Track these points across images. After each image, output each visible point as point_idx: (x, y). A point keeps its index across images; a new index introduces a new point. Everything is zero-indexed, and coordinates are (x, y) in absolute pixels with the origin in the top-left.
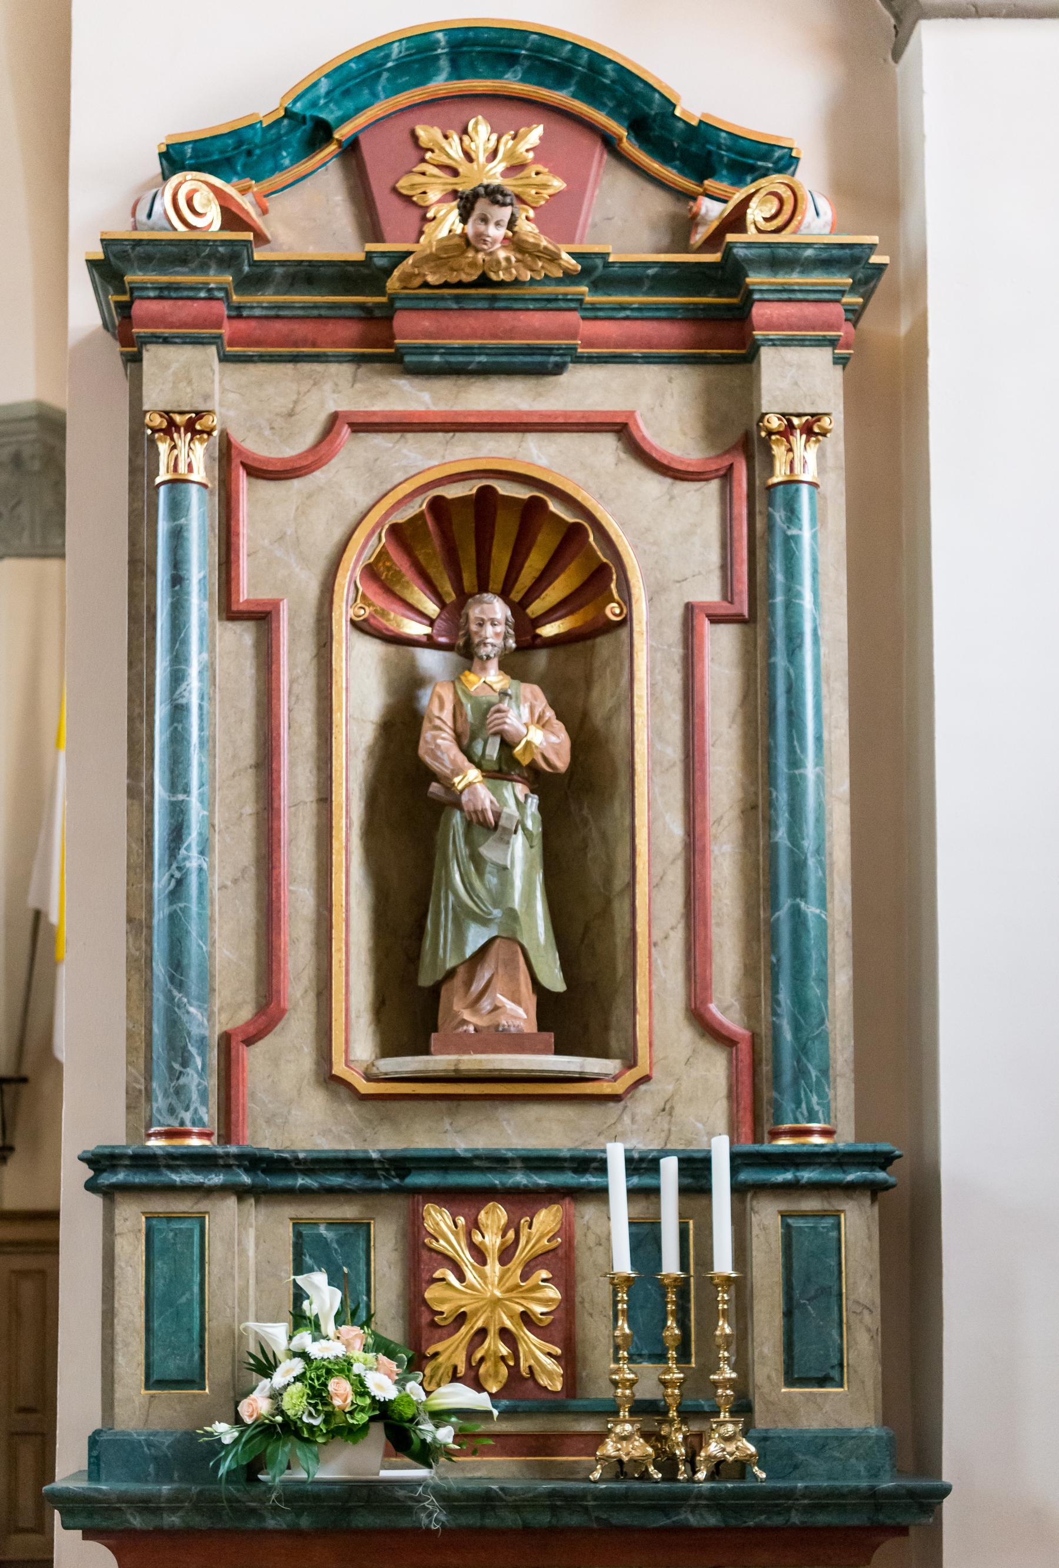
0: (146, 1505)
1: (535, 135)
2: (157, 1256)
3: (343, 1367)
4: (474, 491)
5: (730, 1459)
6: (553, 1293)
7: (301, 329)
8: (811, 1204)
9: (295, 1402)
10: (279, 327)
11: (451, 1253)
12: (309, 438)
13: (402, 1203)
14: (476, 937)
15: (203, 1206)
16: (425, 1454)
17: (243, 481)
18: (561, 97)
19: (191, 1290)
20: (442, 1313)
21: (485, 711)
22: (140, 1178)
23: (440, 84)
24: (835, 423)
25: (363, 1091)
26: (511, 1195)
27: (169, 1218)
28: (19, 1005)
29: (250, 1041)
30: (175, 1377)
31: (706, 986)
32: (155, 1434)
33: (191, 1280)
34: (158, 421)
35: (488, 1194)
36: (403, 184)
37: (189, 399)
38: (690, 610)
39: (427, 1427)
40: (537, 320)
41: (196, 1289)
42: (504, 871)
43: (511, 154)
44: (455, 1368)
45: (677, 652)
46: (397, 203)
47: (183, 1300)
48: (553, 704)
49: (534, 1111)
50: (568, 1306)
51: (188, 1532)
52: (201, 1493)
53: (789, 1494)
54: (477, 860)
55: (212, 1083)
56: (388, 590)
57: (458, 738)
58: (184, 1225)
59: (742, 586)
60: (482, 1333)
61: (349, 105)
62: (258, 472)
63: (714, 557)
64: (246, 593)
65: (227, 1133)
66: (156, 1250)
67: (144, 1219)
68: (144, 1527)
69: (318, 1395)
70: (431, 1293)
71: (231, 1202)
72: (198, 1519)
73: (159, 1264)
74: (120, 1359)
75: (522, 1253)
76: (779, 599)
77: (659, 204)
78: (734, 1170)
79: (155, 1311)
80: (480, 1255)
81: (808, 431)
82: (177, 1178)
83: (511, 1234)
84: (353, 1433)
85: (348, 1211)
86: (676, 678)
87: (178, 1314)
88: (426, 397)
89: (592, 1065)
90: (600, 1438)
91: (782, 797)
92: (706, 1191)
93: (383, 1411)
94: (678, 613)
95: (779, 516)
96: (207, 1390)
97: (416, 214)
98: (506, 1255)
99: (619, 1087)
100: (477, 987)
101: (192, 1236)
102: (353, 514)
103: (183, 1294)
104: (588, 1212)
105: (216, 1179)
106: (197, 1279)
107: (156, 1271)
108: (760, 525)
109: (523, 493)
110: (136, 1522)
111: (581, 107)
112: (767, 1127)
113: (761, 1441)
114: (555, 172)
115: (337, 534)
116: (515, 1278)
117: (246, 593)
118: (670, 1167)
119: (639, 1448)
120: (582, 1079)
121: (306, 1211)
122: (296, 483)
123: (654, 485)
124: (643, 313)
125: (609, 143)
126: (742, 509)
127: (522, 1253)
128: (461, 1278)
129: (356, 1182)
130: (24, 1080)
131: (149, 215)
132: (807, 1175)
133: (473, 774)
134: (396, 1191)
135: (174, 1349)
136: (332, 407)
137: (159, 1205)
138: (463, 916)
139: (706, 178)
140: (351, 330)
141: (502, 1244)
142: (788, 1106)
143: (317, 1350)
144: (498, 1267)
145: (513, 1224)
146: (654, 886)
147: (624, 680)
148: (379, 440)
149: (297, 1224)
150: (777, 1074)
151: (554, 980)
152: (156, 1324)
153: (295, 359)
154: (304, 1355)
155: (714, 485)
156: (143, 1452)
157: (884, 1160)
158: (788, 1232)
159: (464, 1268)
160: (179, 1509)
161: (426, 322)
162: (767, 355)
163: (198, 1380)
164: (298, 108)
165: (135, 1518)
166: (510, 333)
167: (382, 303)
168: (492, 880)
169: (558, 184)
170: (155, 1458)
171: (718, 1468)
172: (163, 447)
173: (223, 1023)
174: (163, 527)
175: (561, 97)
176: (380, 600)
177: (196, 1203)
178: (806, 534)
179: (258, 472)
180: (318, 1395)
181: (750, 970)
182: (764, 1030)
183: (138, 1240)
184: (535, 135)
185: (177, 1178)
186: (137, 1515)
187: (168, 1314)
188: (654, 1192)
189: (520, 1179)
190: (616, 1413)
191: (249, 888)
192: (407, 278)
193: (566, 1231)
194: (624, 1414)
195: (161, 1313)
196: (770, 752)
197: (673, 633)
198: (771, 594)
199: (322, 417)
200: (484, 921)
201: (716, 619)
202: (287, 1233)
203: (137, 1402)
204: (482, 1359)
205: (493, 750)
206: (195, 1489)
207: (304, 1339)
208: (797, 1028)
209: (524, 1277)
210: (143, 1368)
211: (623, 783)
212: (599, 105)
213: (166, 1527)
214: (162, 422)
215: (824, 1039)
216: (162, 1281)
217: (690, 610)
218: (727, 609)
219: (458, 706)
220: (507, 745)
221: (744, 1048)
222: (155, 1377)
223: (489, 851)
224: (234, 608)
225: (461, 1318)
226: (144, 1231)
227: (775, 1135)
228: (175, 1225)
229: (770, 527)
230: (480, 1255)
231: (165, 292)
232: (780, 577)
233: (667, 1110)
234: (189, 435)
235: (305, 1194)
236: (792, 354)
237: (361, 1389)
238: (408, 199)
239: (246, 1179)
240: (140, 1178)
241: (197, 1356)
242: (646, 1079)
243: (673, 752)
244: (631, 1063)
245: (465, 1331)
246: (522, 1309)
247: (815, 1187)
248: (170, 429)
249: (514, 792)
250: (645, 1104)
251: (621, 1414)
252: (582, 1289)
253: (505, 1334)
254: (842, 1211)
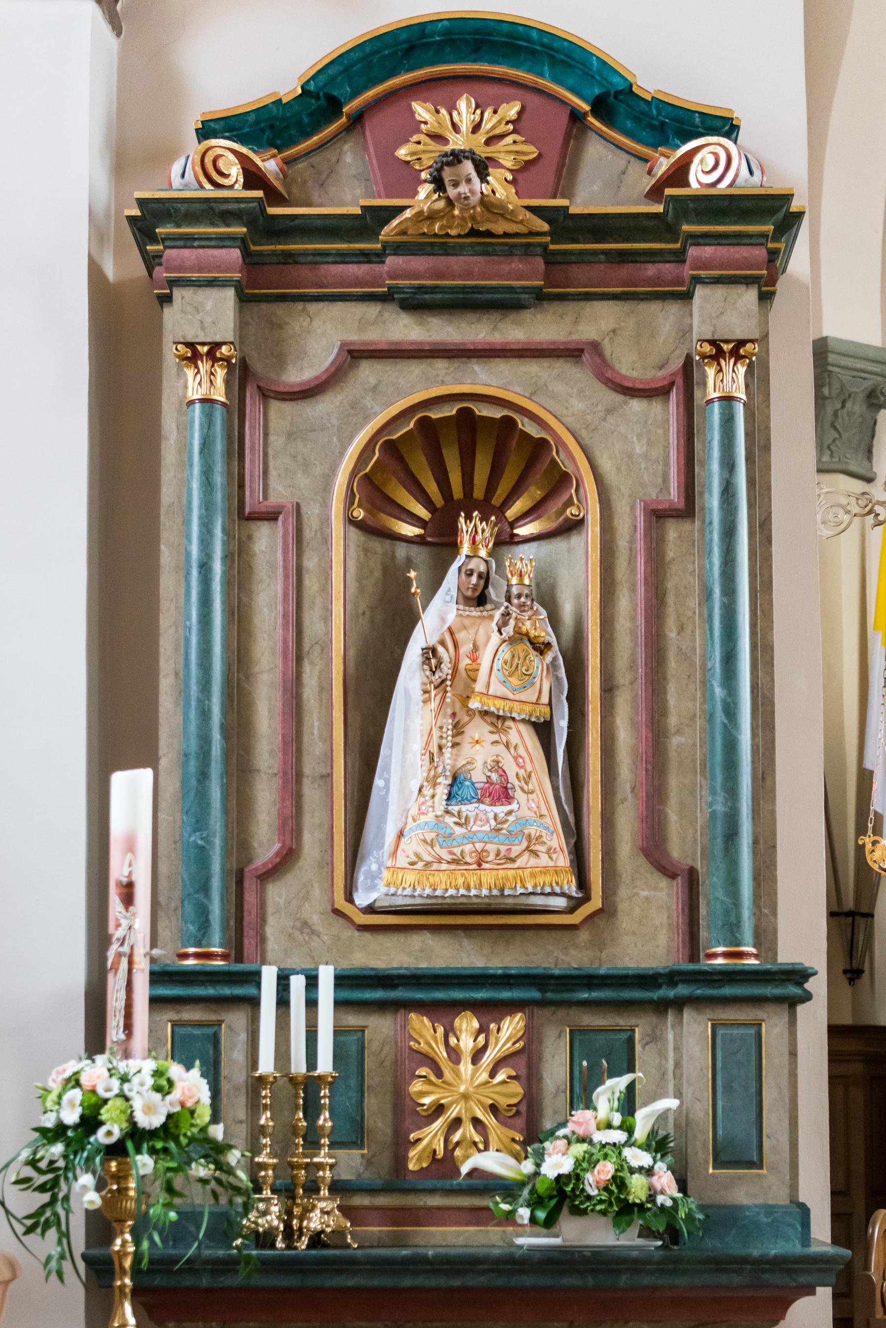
4: (454, 412)
5: (329, 1230)
11: (432, 1054)
20: (423, 1105)
24: (171, 353)
26: (475, 1006)
44: (435, 1151)
60: (457, 1123)
83: (481, 1039)
98: (477, 1056)
116: (484, 1076)
128: (439, 1074)
131: (183, 176)
139: (660, 146)
141: (474, 1046)
144: (470, 1067)
159: (441, 1064)
163: (758, 1163)
164: (312, 87)
167: (677, 249)
171: (317, 1240)
172: (711, 372)
184: (512, 110)
190: (318, 1190)
194: (324, 1192)
204: (458, 1144)
209: (492, 1074)
214: (711, 350)
224: (681, 505)
230: (454, 1055)
234: (732, 361)
246: (491, 1102)
248: (718, 356)
251: (322, 1192)
254: (763, 1020)
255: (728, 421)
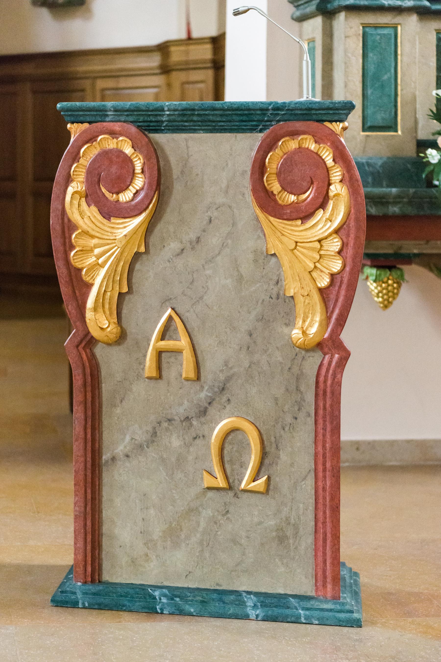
2: (369, 50)
15: (398, 19)
19: (390, 71)
27: (376, 27)
30: (381, 124)
32: (371, 158)
33: (390, 66)
41: (393, 71)
47: (386, 77)
51: (404, 217)
52: (415, 193)
58: (385, 31)
66: (369, 47)
67: (361, 28)
68: (377, 214)
72: (410, 209)
73: (371, 55)
79: (369, 84)
87: (382, 87)
96: (400, 132)
101: (390, 39)
103: (386, 73)
106: (393, 65)
107: (370, 59)
135: (380, 107)
152: (369, 92)
156: (365, 170)
160: (399, 202)
163: (394, 126)
165: (372, 209)
170: (372, 174)
177: (393, 18)
183: (359, 40)
186: (373, 206)
187: (376, 85)
195: (372, 86)
203: (358, 140)
206: (412, 191)
210: (361, 119)
213: (390, 214)
216: (373, 66)
222: (369, 124)
226: (361, 35)
228: (380, 31)
241: (393, 111)
255: (159, 126)
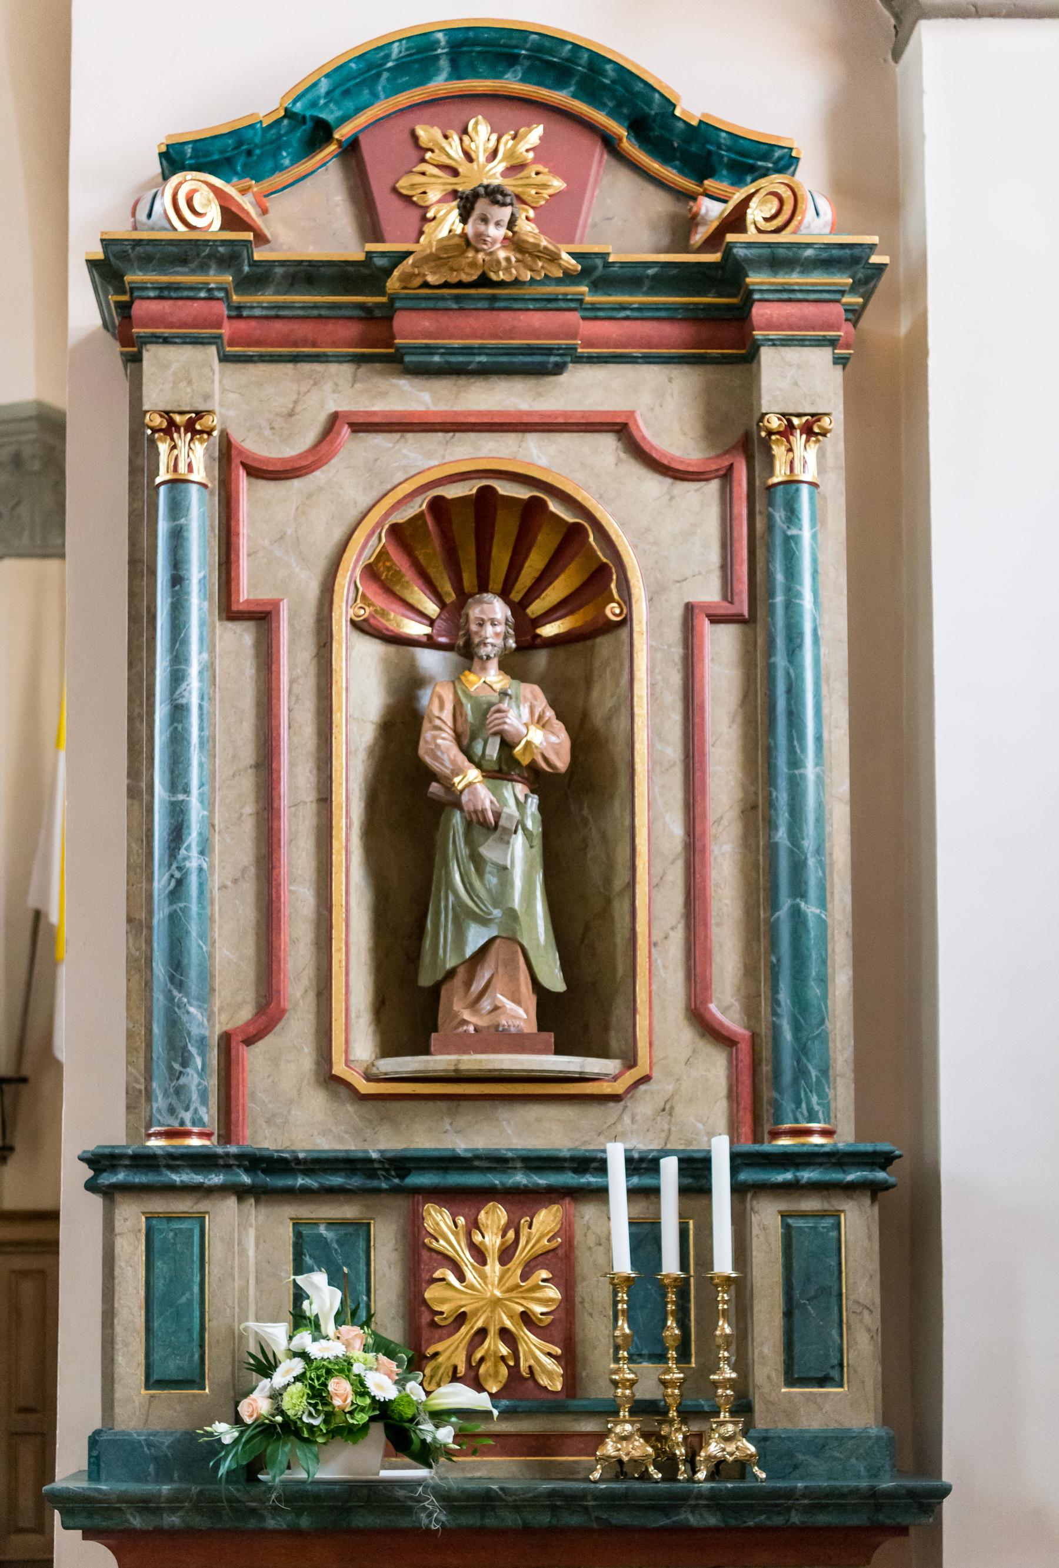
0: (146, 1505)
1: (535, 135)
2: (157, 1256)
3: (343, 1367)
4: (474, 491)
5: (730, 1459)
6: (553, 1293)
7: (301, 329)
8: (811, 1204)
9: (295, 1402)
10: (279, 327)
11: (451, 1253)
12: (309, 438)
13: (402, 1203)
14: (476, 937)
15: (203, 1206)
16: (425, 1454)
17: (243, 481)
18: (561, 97)
19: (191, 1290)
20: (442, 1313)
21: (485, 711)
22: (140, 1178)
23: (440, 84)
24: (835, 423)
25: (363, 1091)
26: (511, 1195)
27: (169, 1218)
28: (19, 1005)
29: (250, 1041)
30: (175, 1377)
31: (706, 986)
32: (155, 1434)
33: (191, 1280)
34: (158, 421)
35: (488, 1194)
36: (403, 184)
37: (189, 399)
38: (690, 610)
39: (427, 1427)
40: (537, 320)
41: (196, 1289)
42: (504, 871)
43: (511, 154)
44: (455, 1368)
45: (677, 652)
46: (397, 203)
47: (183, 1300)
48: (553, 704)
49: (534, 1111)
50: (568, 1306)
51: (188, 1532)
52: (201, 1493)
53: (789, 1494)
54: (477, 860)
55: (212, 1083)
56: (388, 590)
57: (458, 738)
58: (184, 1225)
59: (742, 586)
60: (482, 1333)
61: (349, 105)
62: (258, 472)
63: (714, 557)
64: (246, 593)
65: (227, 1133)
66: (156, 1250)
67: (144, 1219)
68: (144, 1527)
69: (318, 1395)
70: (431, 1293)
71: (231, 1202)
72: (198, 1519)
73: (159, 1264)
74: (120, 1359)
75: (522, 1253)
76: (779, 599)
77: (659, 204)
78: (734, 1170)
79: (155, 1311)
80: (480, 1255)
81: (808, 431)
82: (177, 1178)
83: (511, 1234)
84: (353, 1433)
85: (348, 1211)
86: (676, 678)
87: (178, 1314)
88: (426, 397)
89: (592, 1065)
90: (600, 1438)
91: (782, 797)
92: (706, 1191)
93: (383, 1411)
94: (678, 613)
95: (779, 516)
96: (207, 1390)
97: (416, 214)
98: (506, 1255)
99: (619, 1087)
100: (477, 987)
101: (192, 1236)
102: (353, 514)
103: (183, 1294)
104: (588, 1212)
105: (216, 1179)
106: (197, 1279)
107: (156, 1271)
108: (760, 525)
109: (523, 493)
110: (136, 1522)
111: (581, 107)
112: (767, 1127)
113: (761, 1441)
114: (555, 172)
115: (337, 534)
116: (515, 1278)
117: (246, 593)
118: (670, 1167)
119: (639, 1448)
120: (582, 1079)
121: (306, 1211)
122: (296, 483)
123: (654, 485)
124: (643, 313)
125: (609, 143)
126: (742, 509)
127: (522, 1253)
128: (461, 1278)
129: (356, 1182)
130: (24, 1080)
131: (149, 215)
132: (807, 1175)
133: (473, 774)
134: (396, 1191)
135: (174, 1349)
136: (332, 407)
137: (159, 1205)
138: (463, 916)
139: (706, 178)
140: (351, 330)
141: (502, 1244)
142: (788, 1106)
143: (317, 1350)
144: (498, 1267)
145: (513, 1224)
146: (654, 886)
147: (624, 680)
148: (379, 440)
149: (297, 1224)
150: (777, 1074)
151: (554, 980)
152: (156, 1324)
153: (295, 359)
154: (304, 1355)
155: (714, 485)
156: (143, 1452)
157: (884, 1160)
158: (788, 1232)
159: (464, 1268)
160: (179, 1509)
161: (426, 322)
162: (767, 355)
163: (198, 1380)
164: (298, 108)
165: (135, 1518)
166: (510, 333)
167: (382, 303)
168: (492, 880)
169: (558, 184)
170: (155, 1458)
171: (718, 1468)
172: (163, 447)
173: (223, 1023)
174: (163, 527)
175: (561, 97)
176: (380, 600)
177: (196, 1203)
178: (806, 534)
179: (258, 472)
180: (318, 1395)
181: (750, 970)
182: (764, 1030)
183: (138, 1240)
184: (535, 135)
185: (177, 1178)
186: (137, 1515)
187: (168, 1314)
188: (654, 1192)
189: (520, 1179)
190: (616, 1413)
191: (249, 888)
192: (407, 278)
193: (566, 1231)
194: (624, 1414)
195: (161, 1313)
196: (770, 752)
197: (673, 633)
198: (771, 594)
199: (322, 417)
200: (484, 921)
201: (716, 619)
202: (287, 1233)
203: (137, 1402)
204: (482, 1359)
205: (493, 750)
206: (195, 1489)
207: (304, 1339)
208: (797, 1028)
209: (524, 1277)
210: (143, 1368)
211: (623, 783)
212: (599, 105)
213: (166, 1527)
214: (162, 422)
215: (824, 1039)
216: (162, 1281)
217: (690, 610)
218: (727, 609)
219: (458, 706)
220: (507, 745)
221: (744, 1048)
222: (155, 1377)
223: (489, 851)
224: (234, 608)
225: (461, 1318)
226: (144, 1231)
227: (775, 1135)
228: (175, 1225)
229: (770, 527)
230: (480, 1255)
231: (165, 292)
232: (780, 577)
233: (667, 1110)
234: (189, 435)
235: (305, 1194)
236: (792, 354)
237: (361, 1389)
238: (408, 199)
239: (246, 1179)
240: (140, 1178)
241: (197, 1356)
242: (646, 1079)
243: (673, 752)
244: (631, 1063)
245: (465, 1331)
246: (522, 1309)
247: (815, 1187)
248: (170, 429)
249: (514, 792)
250: (645, 1104)
251: (621, 1414)
252: (582, 1289)
253: (505, 1334)
254: (842, 1211)
